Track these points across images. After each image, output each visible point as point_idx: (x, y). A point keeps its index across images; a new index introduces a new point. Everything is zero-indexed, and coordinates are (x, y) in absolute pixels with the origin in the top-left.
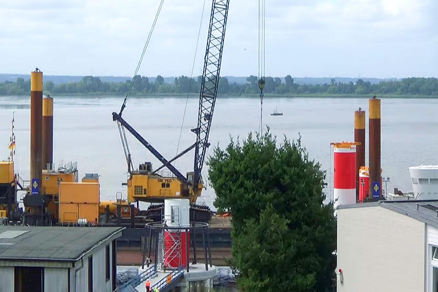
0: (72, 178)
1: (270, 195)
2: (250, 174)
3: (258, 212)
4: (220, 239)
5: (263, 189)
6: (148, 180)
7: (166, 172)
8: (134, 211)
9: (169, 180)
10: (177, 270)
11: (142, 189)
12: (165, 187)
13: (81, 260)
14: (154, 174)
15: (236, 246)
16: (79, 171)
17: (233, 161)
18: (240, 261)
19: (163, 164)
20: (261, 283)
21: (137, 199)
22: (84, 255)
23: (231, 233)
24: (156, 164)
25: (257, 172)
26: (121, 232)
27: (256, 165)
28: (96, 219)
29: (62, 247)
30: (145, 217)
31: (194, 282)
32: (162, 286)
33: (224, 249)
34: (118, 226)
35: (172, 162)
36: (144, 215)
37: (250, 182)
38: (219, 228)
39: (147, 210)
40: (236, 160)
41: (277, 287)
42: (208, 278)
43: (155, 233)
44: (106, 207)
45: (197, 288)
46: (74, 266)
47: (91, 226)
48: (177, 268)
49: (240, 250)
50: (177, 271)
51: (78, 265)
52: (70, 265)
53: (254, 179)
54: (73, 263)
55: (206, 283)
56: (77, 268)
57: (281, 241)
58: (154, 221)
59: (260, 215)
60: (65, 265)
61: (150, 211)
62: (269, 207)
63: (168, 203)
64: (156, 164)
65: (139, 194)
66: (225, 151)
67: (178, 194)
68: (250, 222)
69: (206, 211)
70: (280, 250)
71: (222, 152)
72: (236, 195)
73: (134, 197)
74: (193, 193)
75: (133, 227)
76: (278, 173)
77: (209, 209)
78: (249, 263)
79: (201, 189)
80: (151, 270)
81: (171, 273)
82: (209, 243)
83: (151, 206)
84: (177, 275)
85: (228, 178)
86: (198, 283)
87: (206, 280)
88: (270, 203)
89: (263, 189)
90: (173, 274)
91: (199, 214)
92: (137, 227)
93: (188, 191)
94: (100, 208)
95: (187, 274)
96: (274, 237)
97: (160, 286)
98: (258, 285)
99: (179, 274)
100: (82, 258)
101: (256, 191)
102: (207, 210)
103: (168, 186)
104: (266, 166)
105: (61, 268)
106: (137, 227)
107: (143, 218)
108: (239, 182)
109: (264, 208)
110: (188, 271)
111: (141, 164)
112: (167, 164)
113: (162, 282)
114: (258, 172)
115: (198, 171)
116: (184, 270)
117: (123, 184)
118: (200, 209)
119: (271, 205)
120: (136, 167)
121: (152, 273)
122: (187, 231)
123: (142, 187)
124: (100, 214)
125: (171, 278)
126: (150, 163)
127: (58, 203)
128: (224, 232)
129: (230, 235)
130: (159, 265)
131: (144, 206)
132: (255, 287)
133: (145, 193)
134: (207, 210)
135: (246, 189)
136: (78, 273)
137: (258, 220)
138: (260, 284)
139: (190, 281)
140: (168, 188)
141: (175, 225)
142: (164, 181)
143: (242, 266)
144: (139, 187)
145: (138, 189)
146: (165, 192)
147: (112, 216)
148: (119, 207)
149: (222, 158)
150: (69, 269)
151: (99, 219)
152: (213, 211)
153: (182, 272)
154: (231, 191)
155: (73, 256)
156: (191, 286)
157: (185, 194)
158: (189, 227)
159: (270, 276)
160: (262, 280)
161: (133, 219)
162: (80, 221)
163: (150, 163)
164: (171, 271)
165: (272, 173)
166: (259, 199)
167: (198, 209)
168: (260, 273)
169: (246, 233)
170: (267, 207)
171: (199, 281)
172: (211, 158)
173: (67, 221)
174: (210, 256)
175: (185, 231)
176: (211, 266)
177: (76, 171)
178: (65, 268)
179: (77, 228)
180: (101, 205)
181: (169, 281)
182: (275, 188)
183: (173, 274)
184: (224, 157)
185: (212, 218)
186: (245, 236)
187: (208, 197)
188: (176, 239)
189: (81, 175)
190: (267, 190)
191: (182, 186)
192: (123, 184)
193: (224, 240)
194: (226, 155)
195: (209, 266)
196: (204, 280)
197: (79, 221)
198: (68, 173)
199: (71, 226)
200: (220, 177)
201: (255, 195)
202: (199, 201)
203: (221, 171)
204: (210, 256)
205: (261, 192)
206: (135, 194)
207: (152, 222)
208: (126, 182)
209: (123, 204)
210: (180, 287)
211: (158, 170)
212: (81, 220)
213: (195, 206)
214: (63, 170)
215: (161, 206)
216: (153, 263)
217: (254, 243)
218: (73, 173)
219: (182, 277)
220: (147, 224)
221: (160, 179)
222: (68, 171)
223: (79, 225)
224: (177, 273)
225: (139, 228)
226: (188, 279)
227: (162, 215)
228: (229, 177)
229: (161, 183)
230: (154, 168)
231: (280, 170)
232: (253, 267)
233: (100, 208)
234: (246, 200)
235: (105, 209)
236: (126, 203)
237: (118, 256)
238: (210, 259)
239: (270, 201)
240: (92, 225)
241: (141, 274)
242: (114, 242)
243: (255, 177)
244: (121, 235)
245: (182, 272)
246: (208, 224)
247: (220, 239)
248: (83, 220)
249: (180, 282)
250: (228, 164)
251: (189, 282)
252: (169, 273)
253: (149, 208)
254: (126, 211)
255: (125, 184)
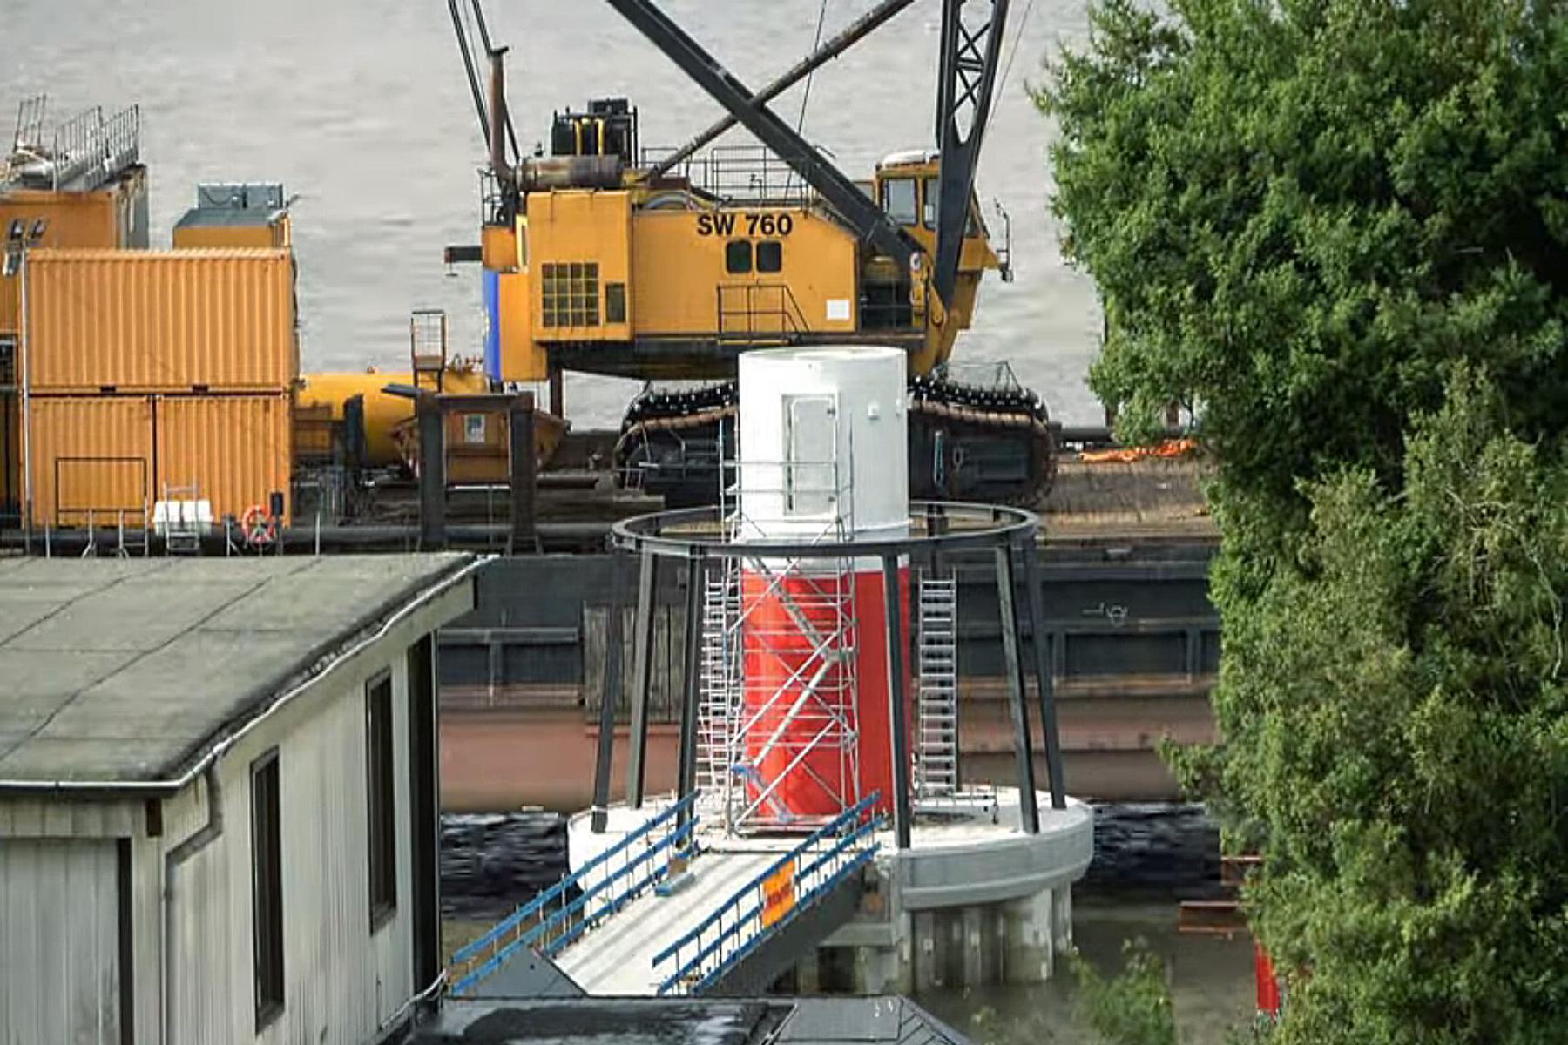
0: (104, 215)
1: (1473, 312)
2: (1336, 166)
3: (1391, 430)
4: (1117, 617)
5: (1422, 270)
6: (631, 221)
7: (742, 167)
8: (534, 434)
9: (773, 217)
10: (830, 832)
11: (592, 287)
12: (749, 268)
13: (203, 783)
14: (658, 180)
15: (1249, 663)
16: (150, 172)
17: (1218, 82)
18: (1274, 764)
19: (725, 113)
20: (1422, 912)
21: (560, 357)
22: (221, 746)
23: (1214, 578)
24: (670, 113)
25: (1380, 154)
26: (469, 586)
27: (1369, 107)
28: (277, 499)
29: (71, 699)
30: (607, 478)
31: (948, 915)
32: (729, 946)
33: (1142, 684)
34: (428, 547)
35: (774, 100)
36: (598, 465)
37: (1332, 224)
38: (1107, 541)
39: (615, 425)
40: (1240, 71)
41: (1523, 933)
42: (1043, 884)
43: (680, 589)
44: (338, 413)
45: (967, 953)
46: (155, 828)
47: (249, 550)
48: (830, 819)
49: (1274, 693)
50: (828, 844)
51: (184, 820)
52: (127, 822)
53: (1363, 204)
54: (152, 804)
55: (1028, 917)
56: (178, 839)
57: (1549, 621)
58: (670, 505)
59: (1404, 450)
60: (93, 823)
61: (639, 437)
62: (1465, 392)
63: (764, 380)
64: (670, 113)
65: (577, 321)
66: (1162, 9)
67: (841, 311)
68: (1341, 495)
69: (1016, 427)
70: (1546, 687)
71: (1147, 23)
72: (1241, 316)
73: (542, 344)
74: (937, 305)
75: (523, 547)
76: (1525, 153)
77: (1041, 415)
78: (1331, 778)
79: (974, 276)
80: (658, 835)
81: (790, 856)
82: (1041, 642)
83: (644, 403)
84: (828, 870)
85: (1184, 199)
86: (974, 915)
87: (1018, 900)
88: (1474, 362)
89: (1422, 270)
90: (807, 860)
91: (973, 446)
92: (554, 544)
93: (902, 289)
94: (305, 420)
95: (901, 860)
96: (1499, 599)
97: (716, 945)
98: (1399, 927)
99: (845, 858)
100: (208, 771)
101: (1373, 288)
102: (1021, 418)
103: (771, 257)
104: (1442, 111)
105: (65, 842)
106: (554, 544)
107: (591, 484)
108: (1259, 227)
109: (1432, 398)
110: (904, 841)
111: (562, 113)
112: (749, 110)
113: (729, 919)
114: (1389, 155)
115: (958, 154)
116: (879, 836)
117: (454, 255)
118: (980, 416)
119: (1481, 373)
120: (532, 134)
121: (661, 859)
122: (891, 562)
123: (592, 269)
124: (303, 461)
125: (786, 890)
126: (624, 103)
127: (17, 395)
128: (1162, 567)
129: (1205, 585)
130: (709, 806)
131: (599, 403)
132: (1379, 940)
133: (616, 316)
134: (1021, 418)
135: (1308, 269)
136: (186, 871)
137: (1393, 480)
138: (1408, 920)
139: (917, 905)
140: (767, 278)
141: (817, 526)
142: (740, 231)
143: (1286, 797)
144: (576, 270)
145: (568, 286)
146: (758, 297)
147: (385, 477)
148: (432, 411)
149: (1141, 64)
150: (124, 847)
151: (297, 494)
152: (1067, 423)
153: (863, 844)
154: (1205, 293)
155: (153, 756)
156: (928, 944)
157: (881, 312)
158: (903, 537)
159: (1482, 864)
160: (1425, 895)
161: (523, 502)
162: (165, 514)
163: (624, 103)
164: (792, 844)
165: (1482, 158)
166: (1400, 338)
167: (967, 414)
168: (1416, 843)
169: (1311, 572)
170: (1455, 391)
171: (982, 906)
172: (1073, 64)
173: (72, 519)
174: (1051, 736)
175: (875, 563)
176: (1059, 804)
177: (131, 169)
178: (97, 843)
179: (124, 566)
180: (305, 398)
181: (775, 914)
182: (1504, 263)
183: (807, 860)
184: (1154, 57)
185: (1063, 469)
186: (1309, 588)
187: (1039, 324)
188: (823, 619)
189: (168, 199)
190: (1452, 277)
191: (864, 256)
192: (454, 255)
193: (1145, 624)
194: (1169, 38)
195: (1043, 799)
196: (1018, 900)
197: (157, 518)
198: (79, 186)
199: (106, 549)
200: (1128, 195)
201: (1369, 310)
202: (973, 356)
203: (1136, 152)
204: (1051, 736)
205: (1410, 293)
206: (548, 322)
207: (653, 507)
208: (476, 240)
209: (459, 389)
210: (849, 952)
211: (684, 155)
212: (174, 506)
213: (945, 393)
214: (43, 167)
215: (712, 398)
216: (663, 791)
217: (1367, 637)
218: (115, 188)
219: (858, 887)
220: (619, 527)
221: (714, 212)
222: (79, 171)
223: (158, 547)
224: (833, 853)
225: (570, 556)
226: (907, 891)
227: (723, 464)
228: (1193, 189)
229: (716, 244)
230: (655, 139)
231: (1541, 137)
232: (1366, 800)
233: (305, 420)
234: (1309, 350)
235: (338, 429)
236: (475, 387)
237: (447, 751)
238: (1053, 755)
239: (1474, 346)
240: (251, 538)
241: (588, 867)
242: (420, 654)
243: (1369, 186)
244: (462, 603)
245: (863, 844)
246: (1032, 518)
247: (1117, 617)
248: (189, 506)
249: (848, 919)
250: (1186, 102)
251: (914, 913)
252: (777, 858)
253: (633, 416)
254: (477, 436)
255: (472, 254)
